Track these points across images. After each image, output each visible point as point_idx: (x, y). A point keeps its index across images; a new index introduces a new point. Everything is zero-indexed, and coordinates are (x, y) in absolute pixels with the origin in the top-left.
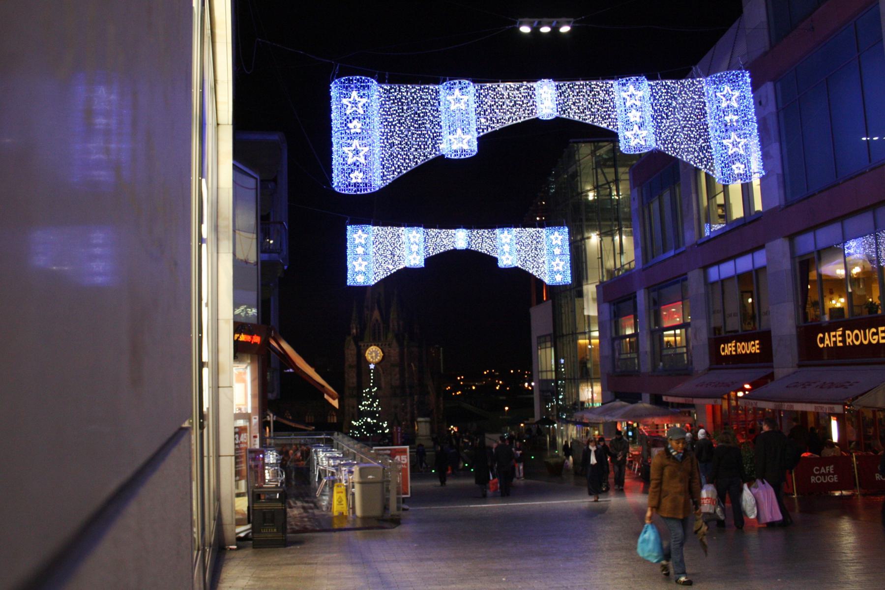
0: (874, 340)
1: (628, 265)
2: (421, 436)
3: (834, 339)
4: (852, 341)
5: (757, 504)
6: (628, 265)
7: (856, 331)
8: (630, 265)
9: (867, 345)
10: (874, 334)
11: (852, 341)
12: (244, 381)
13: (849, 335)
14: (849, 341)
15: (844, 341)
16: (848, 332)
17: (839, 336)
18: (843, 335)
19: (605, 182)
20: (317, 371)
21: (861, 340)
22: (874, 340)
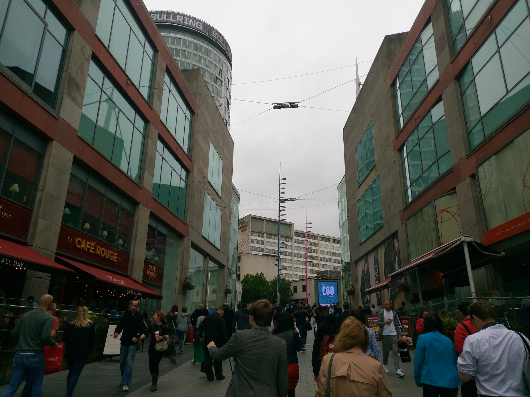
0: (112, 258)
1: (454, 214)
2: (107, 251)
3: (89, 247)
4: (100, 253)
5: (398, 246)
6: (454, 214)
7: (103, 249)
8: (198, 269)
9: (103, 257)
10: (112, 255)
11: (100, 253)
12: (522, 299)
13: (99, 249)
14: (98, 252)
15: (95, 250)
16: (99, 247)
17: (93, 246)
18: (95, 247)
19: (453, 217)
20: (69, 268)
21: (109, 256)
22: (112, 258)
